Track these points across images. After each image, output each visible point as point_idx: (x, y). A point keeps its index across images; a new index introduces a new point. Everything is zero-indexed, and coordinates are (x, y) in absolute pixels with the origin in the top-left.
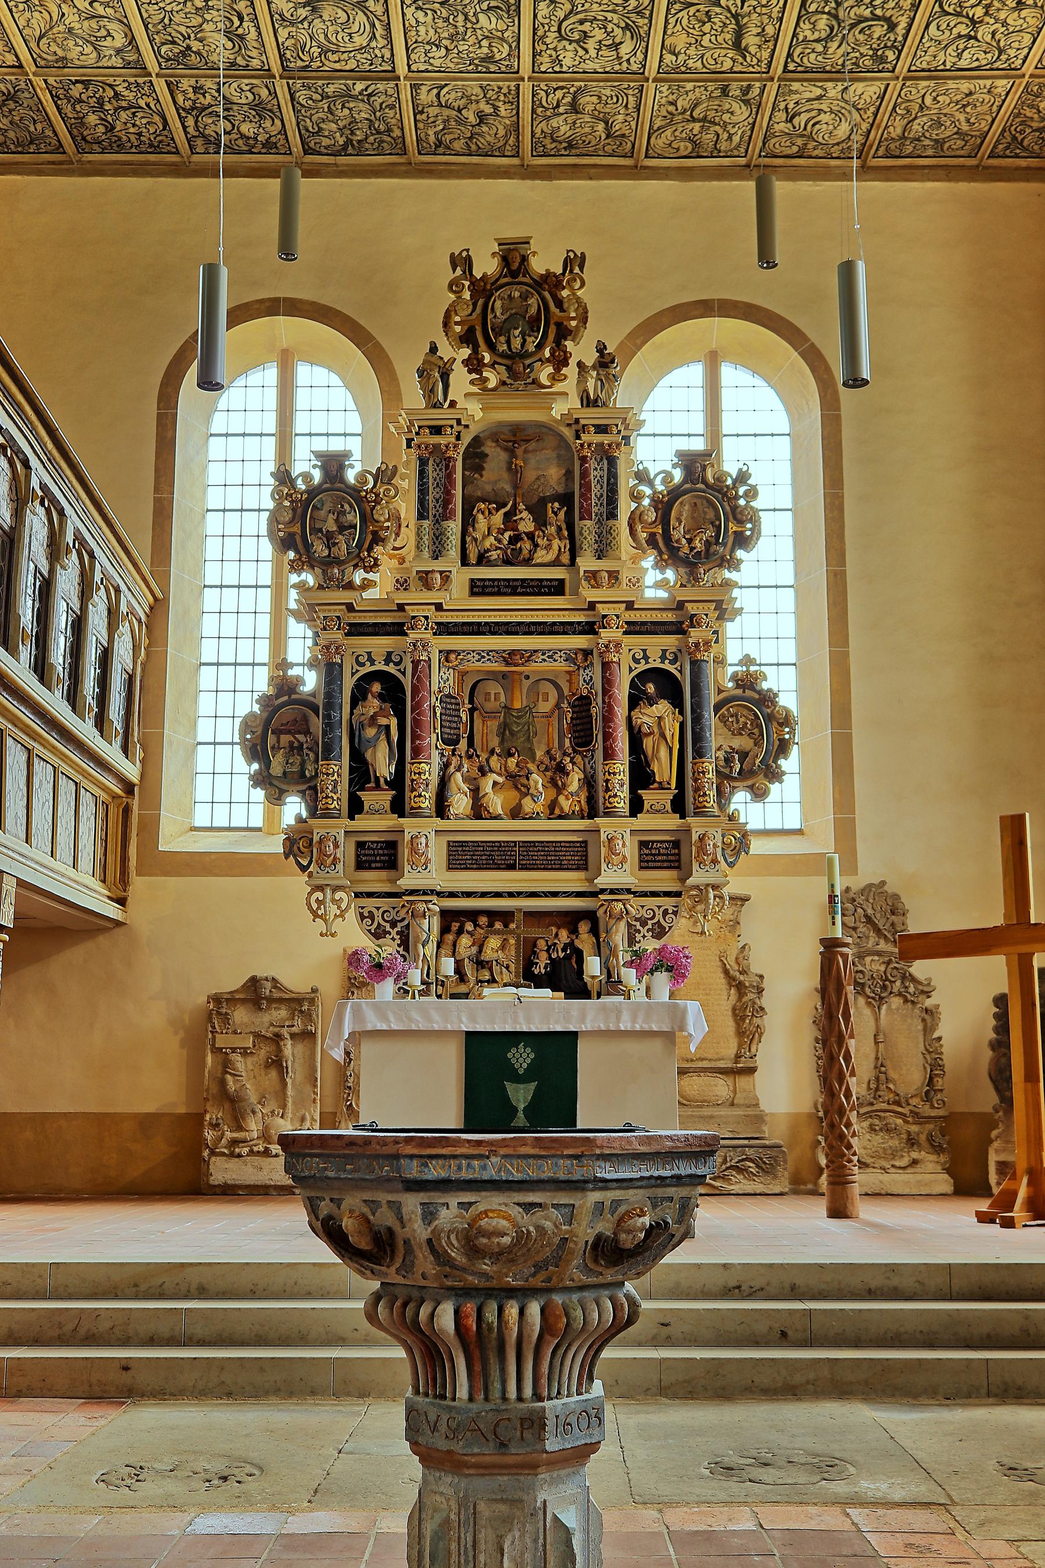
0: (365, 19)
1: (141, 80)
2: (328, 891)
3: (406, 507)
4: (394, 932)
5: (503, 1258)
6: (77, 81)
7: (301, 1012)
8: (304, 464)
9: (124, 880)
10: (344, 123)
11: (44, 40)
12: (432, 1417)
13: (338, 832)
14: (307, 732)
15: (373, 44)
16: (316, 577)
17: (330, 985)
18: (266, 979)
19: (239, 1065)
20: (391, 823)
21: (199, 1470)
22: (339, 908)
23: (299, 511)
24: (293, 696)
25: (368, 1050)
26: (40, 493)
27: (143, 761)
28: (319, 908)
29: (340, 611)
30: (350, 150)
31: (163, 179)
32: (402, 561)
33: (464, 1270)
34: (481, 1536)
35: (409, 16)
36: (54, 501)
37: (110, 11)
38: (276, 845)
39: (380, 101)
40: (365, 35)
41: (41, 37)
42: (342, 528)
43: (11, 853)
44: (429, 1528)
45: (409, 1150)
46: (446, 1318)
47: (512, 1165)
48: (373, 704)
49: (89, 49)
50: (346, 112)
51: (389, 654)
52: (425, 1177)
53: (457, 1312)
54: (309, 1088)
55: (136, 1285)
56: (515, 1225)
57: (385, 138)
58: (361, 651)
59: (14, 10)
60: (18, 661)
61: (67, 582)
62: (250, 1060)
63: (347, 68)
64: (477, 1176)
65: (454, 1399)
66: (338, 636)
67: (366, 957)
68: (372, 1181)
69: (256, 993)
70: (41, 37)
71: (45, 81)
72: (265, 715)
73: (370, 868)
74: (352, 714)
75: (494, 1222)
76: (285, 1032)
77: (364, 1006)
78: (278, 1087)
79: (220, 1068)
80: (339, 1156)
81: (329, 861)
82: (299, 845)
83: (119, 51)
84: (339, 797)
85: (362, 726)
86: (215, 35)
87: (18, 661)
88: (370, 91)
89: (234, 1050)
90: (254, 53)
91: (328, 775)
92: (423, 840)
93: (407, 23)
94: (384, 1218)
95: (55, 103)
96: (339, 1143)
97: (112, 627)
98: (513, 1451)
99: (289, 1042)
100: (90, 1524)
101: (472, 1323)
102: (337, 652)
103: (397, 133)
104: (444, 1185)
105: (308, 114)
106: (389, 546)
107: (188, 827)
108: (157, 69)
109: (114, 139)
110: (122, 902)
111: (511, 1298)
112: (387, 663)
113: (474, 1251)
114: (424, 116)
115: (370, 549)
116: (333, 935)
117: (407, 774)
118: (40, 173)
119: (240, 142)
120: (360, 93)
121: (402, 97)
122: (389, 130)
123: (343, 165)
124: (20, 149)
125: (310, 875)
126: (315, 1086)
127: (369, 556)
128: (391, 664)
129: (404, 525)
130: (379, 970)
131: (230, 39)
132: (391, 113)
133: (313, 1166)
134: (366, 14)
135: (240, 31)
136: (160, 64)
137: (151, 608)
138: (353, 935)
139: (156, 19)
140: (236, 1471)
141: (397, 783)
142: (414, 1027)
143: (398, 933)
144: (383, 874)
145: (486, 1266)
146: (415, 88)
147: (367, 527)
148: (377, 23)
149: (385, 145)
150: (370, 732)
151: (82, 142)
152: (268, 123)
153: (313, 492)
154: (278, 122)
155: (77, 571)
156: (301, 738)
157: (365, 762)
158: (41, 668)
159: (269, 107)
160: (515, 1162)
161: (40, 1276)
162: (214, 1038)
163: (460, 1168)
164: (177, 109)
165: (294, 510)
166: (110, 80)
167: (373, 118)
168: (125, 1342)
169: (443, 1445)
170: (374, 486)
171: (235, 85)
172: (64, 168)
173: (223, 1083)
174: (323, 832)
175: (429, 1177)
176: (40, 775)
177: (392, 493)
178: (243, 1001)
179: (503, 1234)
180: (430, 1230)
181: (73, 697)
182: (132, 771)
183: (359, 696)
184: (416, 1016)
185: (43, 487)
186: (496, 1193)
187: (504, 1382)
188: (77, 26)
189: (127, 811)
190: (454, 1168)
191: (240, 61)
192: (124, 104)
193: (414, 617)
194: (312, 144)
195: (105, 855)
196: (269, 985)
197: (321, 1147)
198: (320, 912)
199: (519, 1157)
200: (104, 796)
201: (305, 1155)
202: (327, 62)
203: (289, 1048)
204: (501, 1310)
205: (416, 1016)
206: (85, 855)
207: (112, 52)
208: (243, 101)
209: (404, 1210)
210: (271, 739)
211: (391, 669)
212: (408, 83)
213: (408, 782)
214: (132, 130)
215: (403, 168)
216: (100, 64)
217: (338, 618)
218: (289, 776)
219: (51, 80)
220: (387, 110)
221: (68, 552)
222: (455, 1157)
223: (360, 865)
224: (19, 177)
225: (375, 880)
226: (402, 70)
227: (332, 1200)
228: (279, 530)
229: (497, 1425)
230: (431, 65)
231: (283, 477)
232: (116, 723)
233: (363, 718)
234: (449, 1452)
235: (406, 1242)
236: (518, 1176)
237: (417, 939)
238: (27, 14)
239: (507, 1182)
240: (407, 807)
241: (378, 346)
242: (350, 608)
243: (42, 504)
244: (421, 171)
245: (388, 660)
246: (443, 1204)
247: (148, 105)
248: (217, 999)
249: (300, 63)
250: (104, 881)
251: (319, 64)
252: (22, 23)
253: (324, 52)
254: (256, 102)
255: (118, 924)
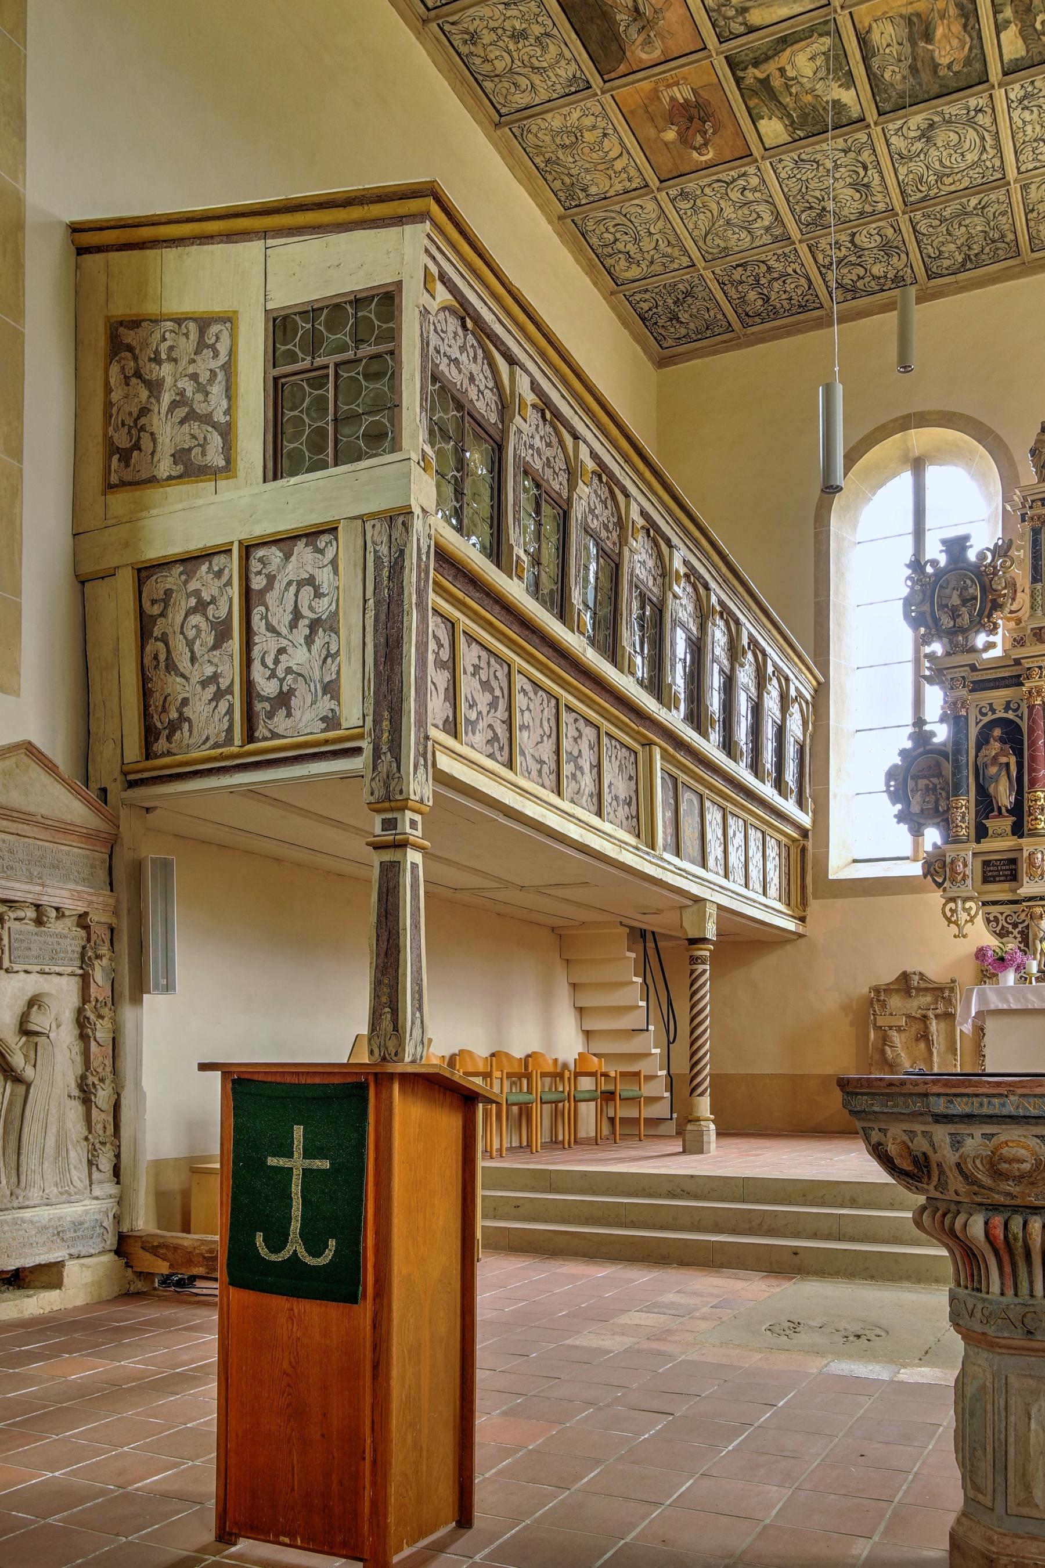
0: (975, 134)
1: (787, 250)
2: (960, 902)
3: (1021, 574)
4: (1015, 932)
5: (1025, 1181)
6: (738, 266)
7: (943, 998)
8: (935, 552)
9: (804, 903)
10: (962, 240)
11: (709, 237)
12: (970, 1306)
13: (968, 857)
14: (940, 775)
15: (984, 157)
16: (944, 646)
17: (966, 975)
18: (915, 973)
19: (895, 1039)
20: (1012, 843)
21: (841, 1328)
22: (969, 914)
23: (928, 592)
24: (928, 748)
25: (990, 1025)
26: (718, 608)
27: (814, 812)
28: (952, 916)
29: (965, 672)
30: (969, 265)
31: (812, 333)
32: (1019, 621)
33: (990, 1189)
34: (1012, 1402)
35: (1016, 118)
36: (731, 614)
37: (758, 195)
38: (916, 869)
39: (993, 210)
40: (976, 151)
41: (706, 235)
42: (964, 601)
43: (712, 886)
44: (970, 1390)
45: (936, 1089)
46: (976, 1227)
47: (1029, 1103)
48: (995, 746)
49: (744, 234)
50: (963, 229)
51: (1008, 703)
52: (950, 1112)
53: (986, 1223)
54: (950, 1057)
55: (804, 1196)
56: (1034, 1153)
57: (1000, 245)
58: (983, 704)
59: (684, 217)
60: (708, 740)
61: (745, 676)
62: (903, 1035)
63: (962, 187)
64: (997, 1112)
65: (988, 1293)
66: (964, 693)
67: (990, 953)
68: (908, 1114)
69: (905, 984)
70: (706, 235)
71: (713, 272)
72: (905, 765)
73: (994, 881)
74: (977, 756)
75: (1014, 1151)
76: (931, 1014)
77: (988, 991)
78: (926, 1055)
79: (880, 1042)
80: (882, 1094)
81: (959, 878)
82: (939, 869)
83: (767, 229)
84: (965, 827)
85: (985, 766)
86: (845, 190)
87: (708, 740)
88: (983, 203)
89: (891, 1028)
90: (879, 197)
91: (957, 808)
92: (1039, 855)
93: (1014, 126)
94: (921, 1145)
95: (722, 289)
96: (881, 1084)
97: (784, 709)
98: (1039, 1338)
99: (934, 1022)
100: (755, 1360)
101: (999, 1233)
102: (963, 707)
103: (1010, 237)
104: (969, 1118)
105: (929, 241)
106: (1007, 610)
107: (850, 859)
108: (799, 236)
109: (770, 308)
110: (802, 919)
111: (1036, 1214)
112: (1006, 712)
113: (998, 1174)
114: (1035, 214)
115: (990, 615)
116: (964, 936)
117: (1025, 802)
118: (716, 353)
119: (873, 283)
120: (975, 209)
121: (1014, 200)
122: (1003, 236)
123: (963, 281)
124: (699, 337)
125: (944, 890)
126: (956, 1055)
127: (989, 621)
128: (1010, 712)
129: (1019, 589)
130: (1002, 962)
131: (858, 191)
132: (1004, 219)
133: (862, 1103)
134: (975, 129)
135: (866, 180)
136: (801, 230)
137: (816, 691)
138: (980, 935)
139: (795, 191)
140: (867, 1332)
141: (1018, 811)
142: (1030, 1007)
143: (1019, 933)
144: (1006, 886)
145: (1009, 1187)
146: (1025, 188)
147: (987, 597)
148: (986, 134)
149: (1000, 252)
150: (993, 770)
151: (746, 318)
152: (895, 259)
153: (940, 573)
154: (903, 256)
155: (753, 668)
156: (935, 780)
157: (989, 796)
158: (728, 746)
159: (895, 244)
160: (1031, 1100)
161: (736, 1186)
162: (875, 1019)
163: (981, 1105)
164: (818, 268)
165: (924, 593)
166: (763, 257)
167: (987, 229)
168: (796, 1235)
169: (978, 1327)
170: (993, 560)
171: (865, 232)
172: (735, 344)
173: (883, 1052)
174: (953, 855)
175: (955, 1112)
176: (733, 827)
177: (1008, 564)
178: (897, 991)
179: (1023, 1161)
180: (957, 1155)
181: (755, 767)
182: (805, 820)
183: (983, 740)
184: (1031, 997)
185: (721, 603)
186: (1016, 1126)
187: (1031, 1283)
188: (733, 216)
189: (804, 850)
190: (976, 1105)
191: (868, 209)
192: (776, 275)
193: (1029, 669)
194: (934, 269)
195: (789, 885)
196: (916, 978)
197: (868, 1087)
198: (953, 919)
199: (1035, 1096)
200: (784, 840)
201: (857, 1094)
202: (942, 187)
203: (934, 1026)
204: (1025, 1224)
205: (1031, 997)
206: (773, 885)
207: (762, 232)
208: (873, 245)
209: (935, 1139)
210: (911, 784)
211: (1010, 715)
212: (1018, 186)
213: (1026, 808)
214: (784, 297)
215: (1017, 269)
216: (754, 245)
217: (963, 678)
218: (926, 812)
219: (717, 271)
220: (1000, 218)
221: (744, 653)
222: (977, 1095)
223: (986, 880)
224: (700, 360)
225: (999, 891)
226: (1012, 173)
227: (880, 1130)
228: (912, 611)
229: (1024, 1316)
230: (1040, 161)
231: (917, 565)
232: (791, 783)
233: (985, 759)
234: (984, 1334)
235: (939, 1165)
236: (1034, 1112)
237: (1035, 936)
238: (694, 218)
239: (1025, 1117)
240: (1026, 829)
241: (998, 438)
242: (973, 668)
243: (722, 617)
244: (1034, 268)
245: (1007, 708)
246: (969, 1135)
247: (795, 271)
248: (877, 990)
249: (919, 195)
250: (789, 905)
251: (936, 191)
252: (691, 226)
253: (940, 178)
254: (884, 242)
255: (801, 936)
